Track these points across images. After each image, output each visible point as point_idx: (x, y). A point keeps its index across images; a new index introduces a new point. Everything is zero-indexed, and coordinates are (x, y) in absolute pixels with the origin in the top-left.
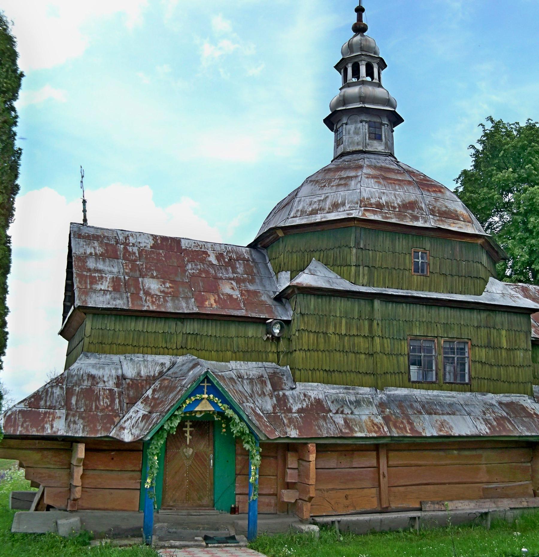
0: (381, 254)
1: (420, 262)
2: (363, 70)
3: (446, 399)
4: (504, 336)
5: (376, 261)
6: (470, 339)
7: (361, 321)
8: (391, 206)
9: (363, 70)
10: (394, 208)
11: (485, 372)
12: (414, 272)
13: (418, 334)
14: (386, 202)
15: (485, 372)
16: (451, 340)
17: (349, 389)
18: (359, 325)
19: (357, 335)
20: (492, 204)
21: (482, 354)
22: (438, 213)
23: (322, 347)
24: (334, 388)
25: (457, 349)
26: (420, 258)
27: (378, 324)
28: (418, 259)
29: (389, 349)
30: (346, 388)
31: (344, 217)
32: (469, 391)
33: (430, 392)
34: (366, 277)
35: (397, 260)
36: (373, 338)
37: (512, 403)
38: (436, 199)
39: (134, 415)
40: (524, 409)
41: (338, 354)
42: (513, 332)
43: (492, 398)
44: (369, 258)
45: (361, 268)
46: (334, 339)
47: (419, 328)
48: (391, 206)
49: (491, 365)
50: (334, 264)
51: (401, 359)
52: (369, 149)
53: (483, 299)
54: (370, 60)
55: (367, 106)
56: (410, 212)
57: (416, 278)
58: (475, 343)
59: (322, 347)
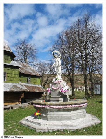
21: (9, 75)
31: (8, 51)
39: (15, 137)
40: (17, 86)
43: (10, 84)
53: (10, 64)
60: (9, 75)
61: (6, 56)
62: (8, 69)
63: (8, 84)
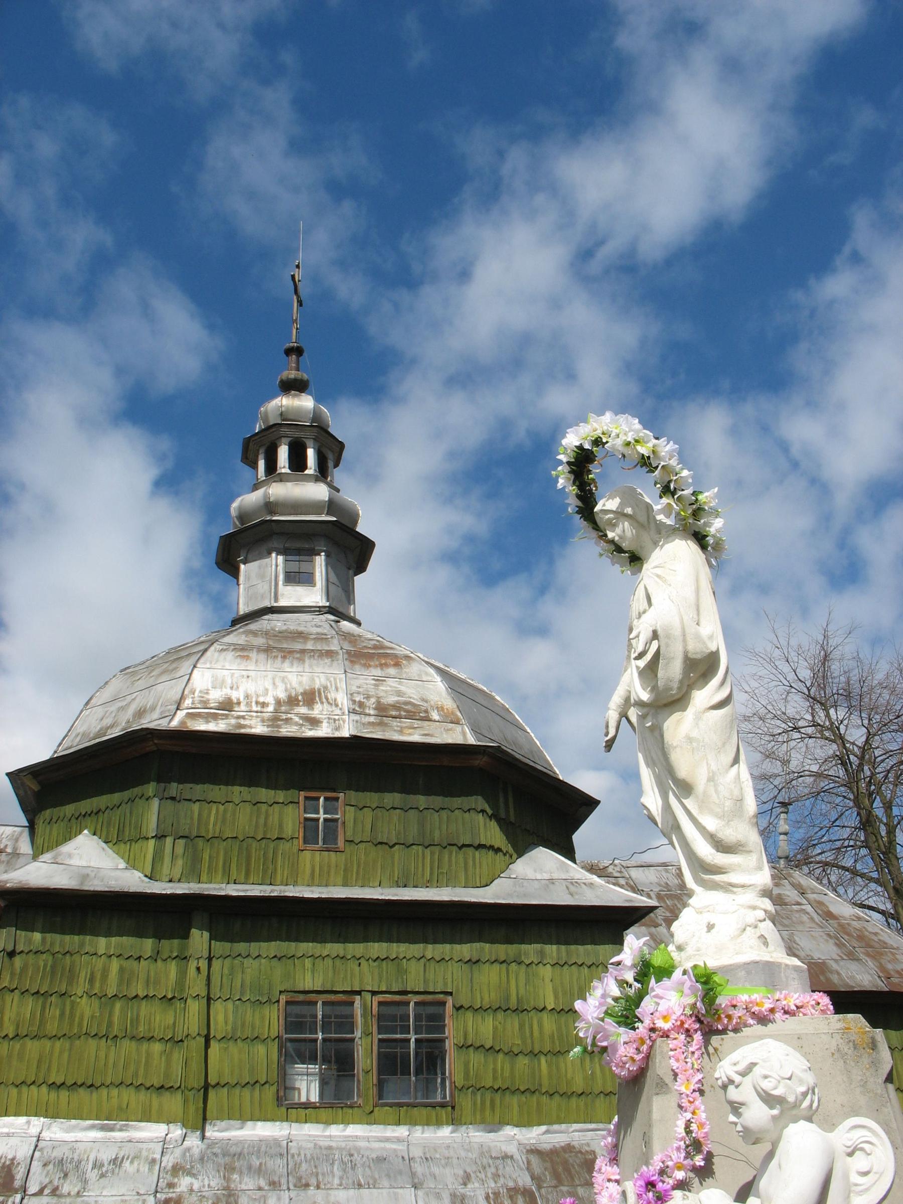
0: (222, 808)
1: (321, 820)
2: (283, 453)
3: (376, 1145)
4: (547, 980)
5: (207, 824)
6: (451, 994)
7: (159, 961)
8: (257, 703)
9: (283, 453)
10: (264, 705)
11: (495, 1070)
12: (305, 842)
13: (308, 986)
14: (247, 696)
15: (495, 1070)
16: (397, 998)
17: (111, 1129)
18: (152, 974)
19: (146, 996)
20: (796, 729)
21: (485, 1028)
22: (375, 709)
23: (52, 1027)
24: (69, 1130)
25: (418, 1017)
26: (321, 811)
27: (198, 969)
28: (318, 813)
29: (229, 1028)
30: (103, 1128)
32: (447, 1124)
33: (335, 1130)
34: (180, 862)
35: (262, 821)
36: (184, 1000)
37: (568, 1148)
38: (379, 681)
41: (93, 1043)
42: (330, 962)
43: (513, 1138)
44: (192, 818)
45: (169, 841)
46: (87, 1008)
47: (313, 972)
48: (257, 703)
49: (512, 1054)
50: (118, 838)
51: (261, 1049)
52: (283, 603)
53: (495, 893)
54: (297, 434)
55: (274, 518)
56: (303, 710)
57: (309, 859)
58: (464, 1001)
59: (52, 1027)
60: (485, 1028)
61: (437, 801)
62: (465, 950)
63: (476, 1136)
